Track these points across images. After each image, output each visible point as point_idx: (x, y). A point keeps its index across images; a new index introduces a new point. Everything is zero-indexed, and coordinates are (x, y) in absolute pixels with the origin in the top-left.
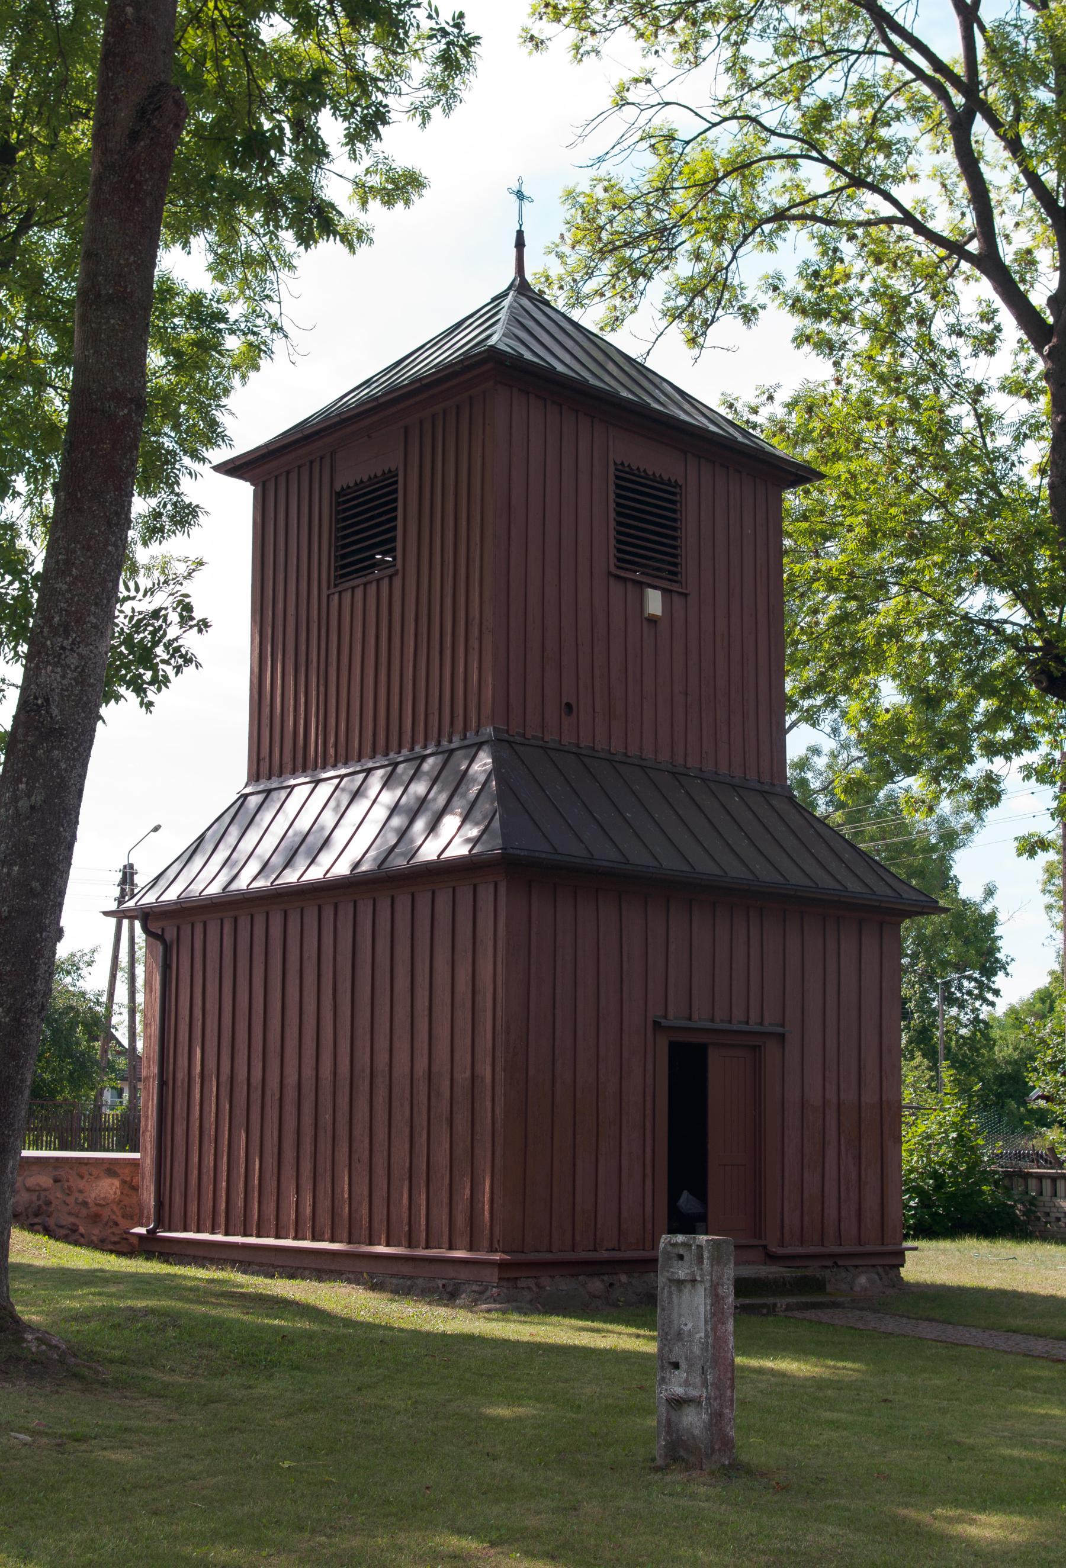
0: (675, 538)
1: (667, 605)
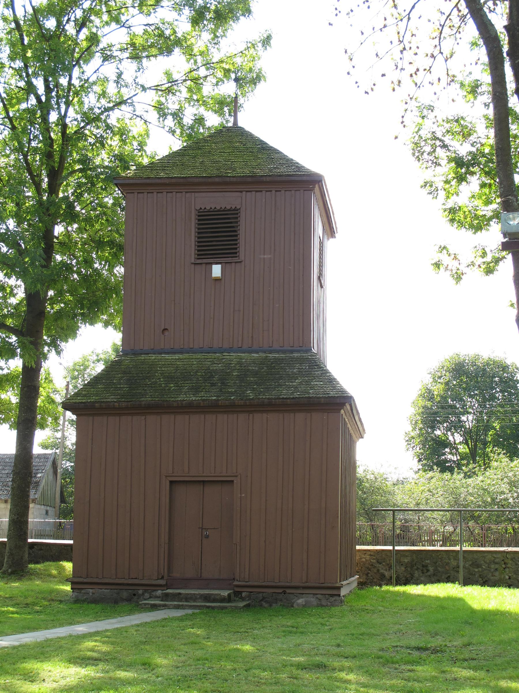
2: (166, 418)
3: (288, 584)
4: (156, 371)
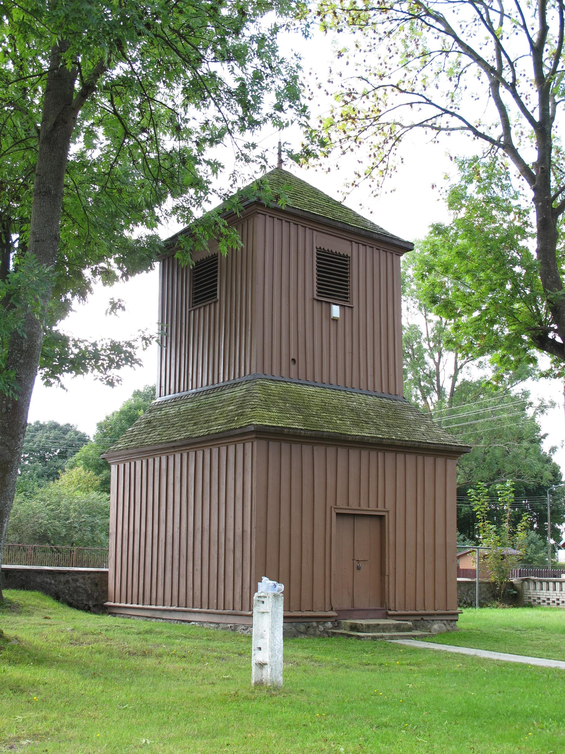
0: (347, 281)
1: (343, 313)
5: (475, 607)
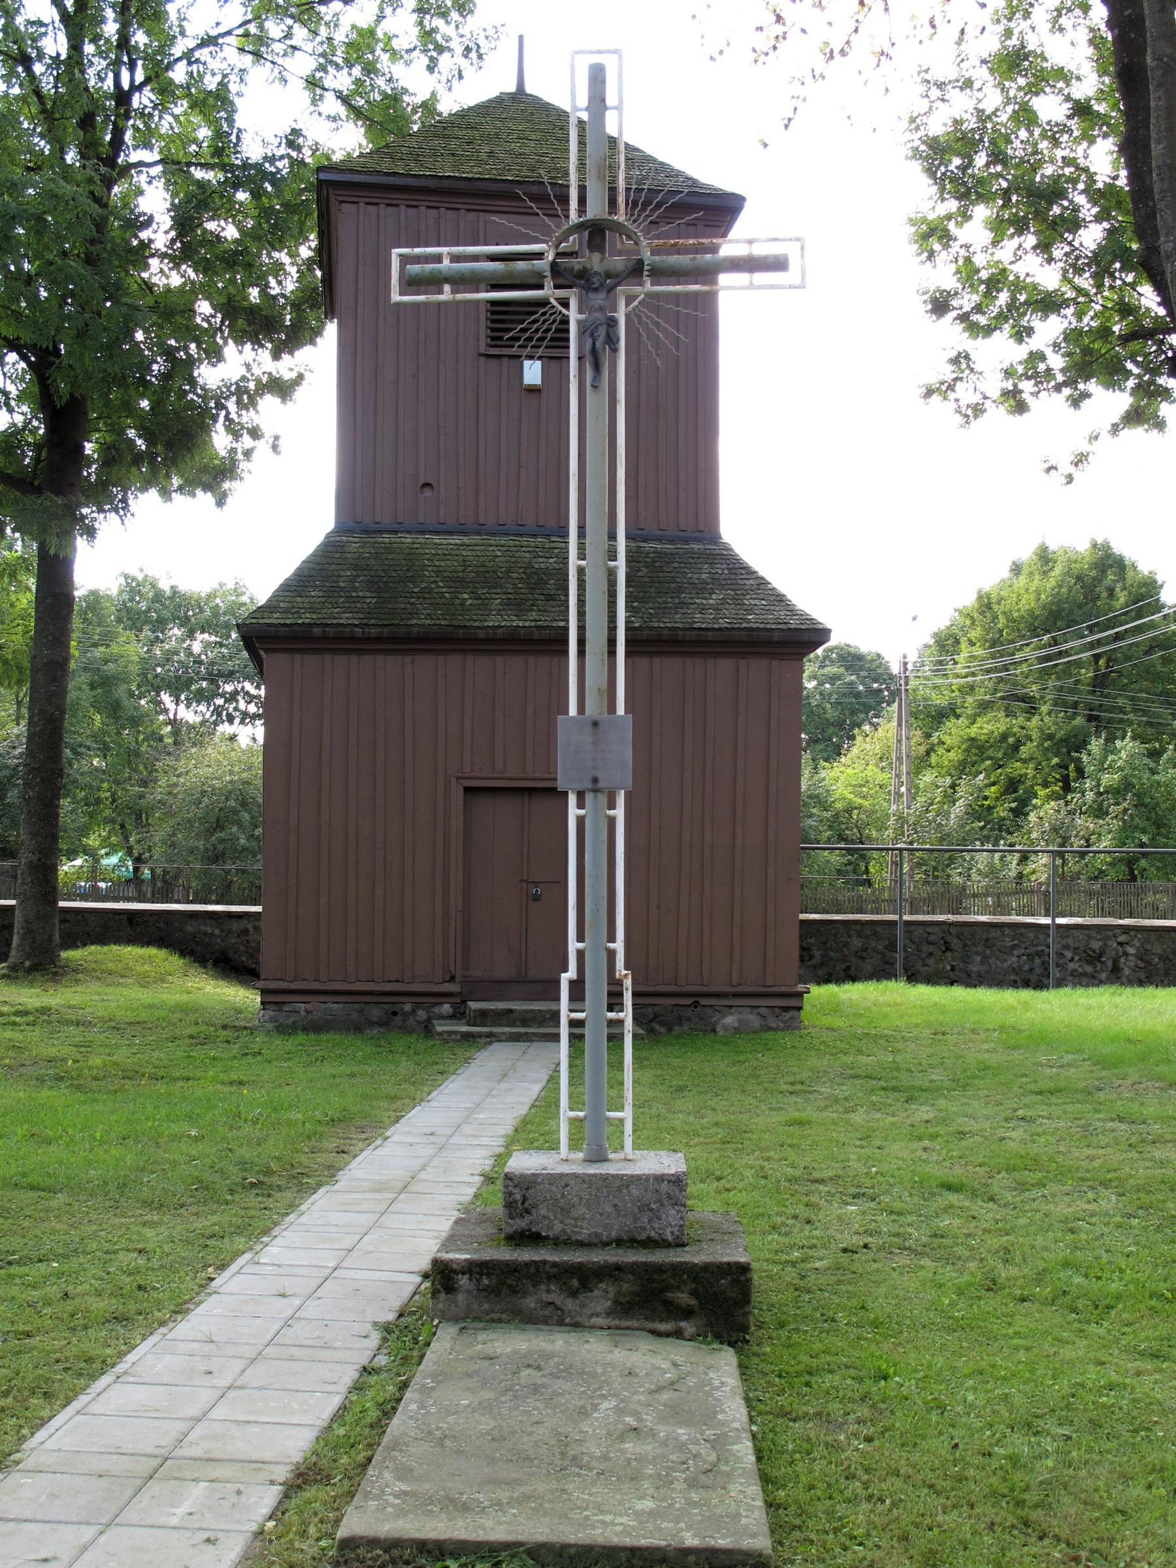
2: (454, 661)
3: (705, 989)
4: (424, 567)
5: (1047, 987)
